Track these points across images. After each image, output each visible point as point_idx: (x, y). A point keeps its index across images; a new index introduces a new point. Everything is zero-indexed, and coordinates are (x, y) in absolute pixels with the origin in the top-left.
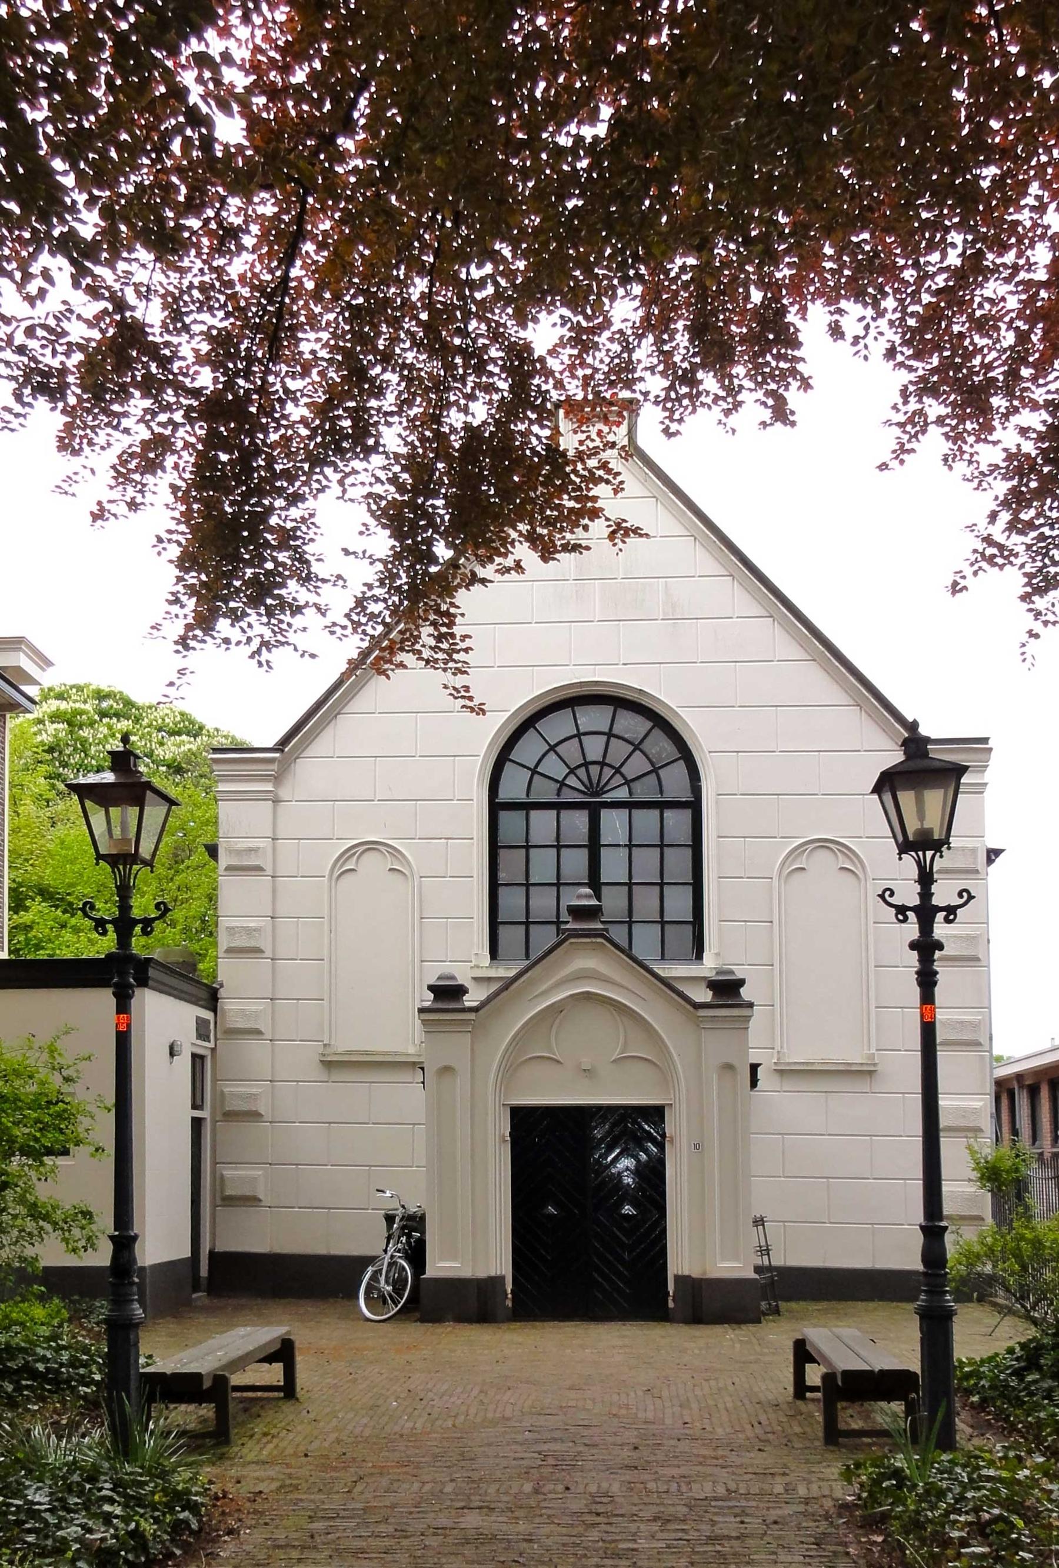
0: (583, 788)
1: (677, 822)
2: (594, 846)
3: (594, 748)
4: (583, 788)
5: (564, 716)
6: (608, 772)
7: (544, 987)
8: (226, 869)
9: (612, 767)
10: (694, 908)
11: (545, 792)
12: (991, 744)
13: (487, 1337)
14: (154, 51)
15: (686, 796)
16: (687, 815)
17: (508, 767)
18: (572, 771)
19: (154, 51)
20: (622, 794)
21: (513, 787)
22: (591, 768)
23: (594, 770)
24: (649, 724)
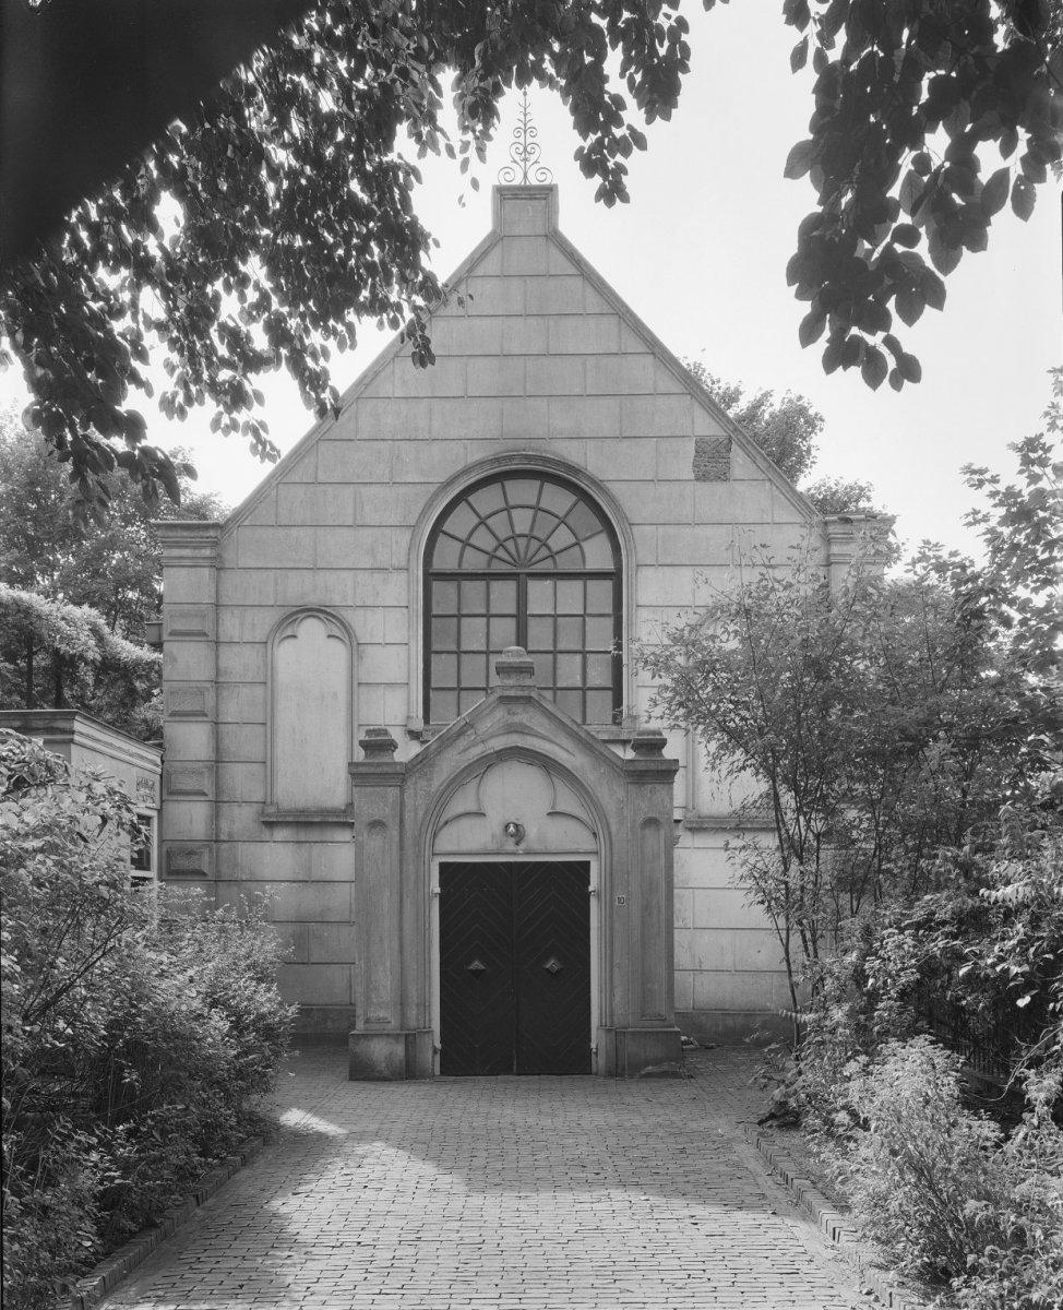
0: (510, 559)
1: (601, 591)
2: (521, 618)
3: (522, 521)
4: (510, 559)
5: (493, 491)
6: (544, 552)
7: (618, 992)
8: (171, 634)
9: (549, 548)
10: (434, 546)
11: (474, 562)
12: (348, 350)
13: (204, 738)
14: (124, 228)
15: (609, 566)
16: (608, 585)
17: (442, 539)
18: (501, 545)
19: (124, 228)
20: (547, 566)
21: (447, 558)
22: (550, 561)
23: (522, 542)
24: (537, 483)
